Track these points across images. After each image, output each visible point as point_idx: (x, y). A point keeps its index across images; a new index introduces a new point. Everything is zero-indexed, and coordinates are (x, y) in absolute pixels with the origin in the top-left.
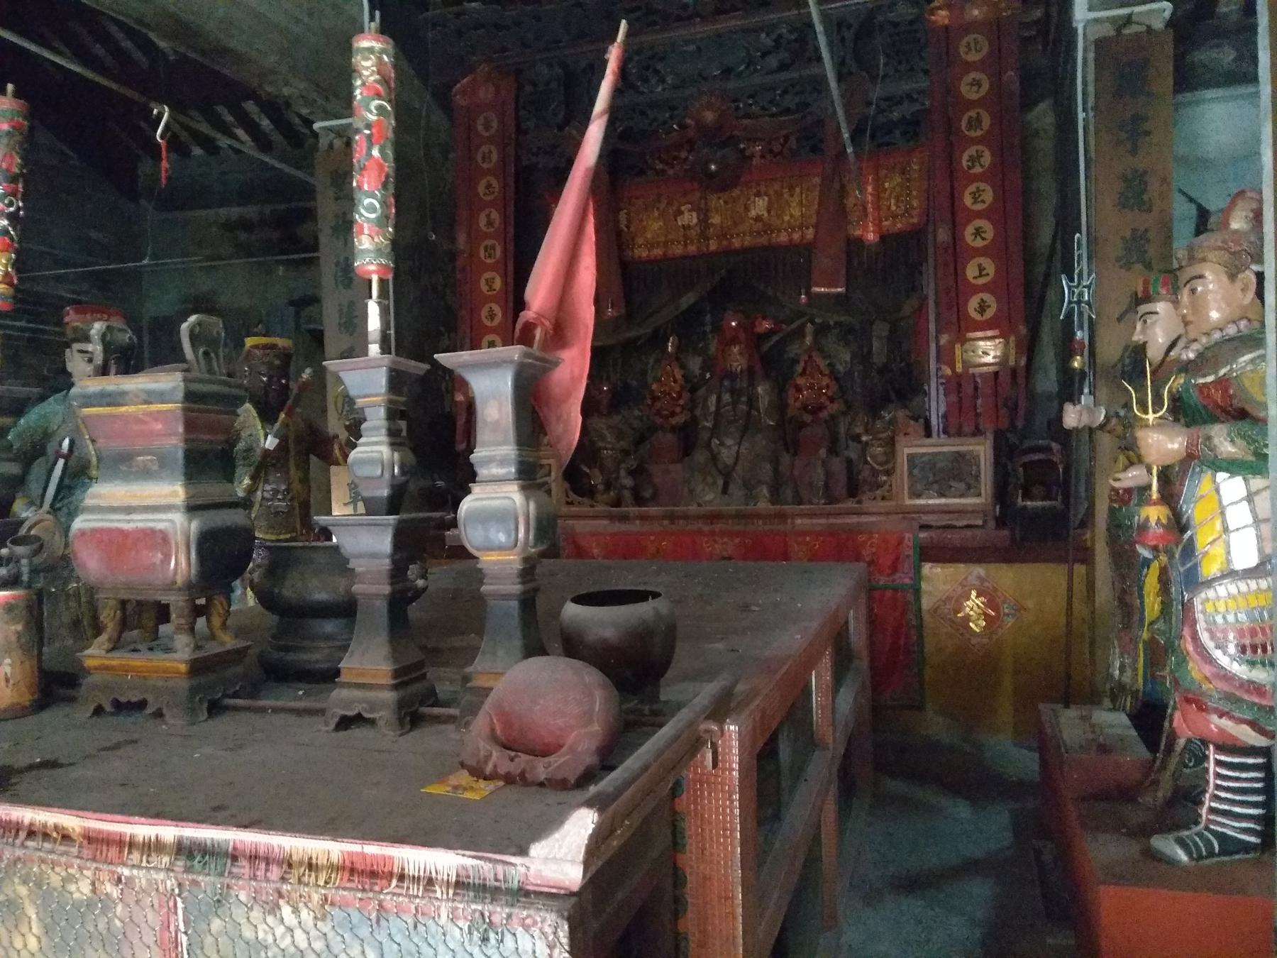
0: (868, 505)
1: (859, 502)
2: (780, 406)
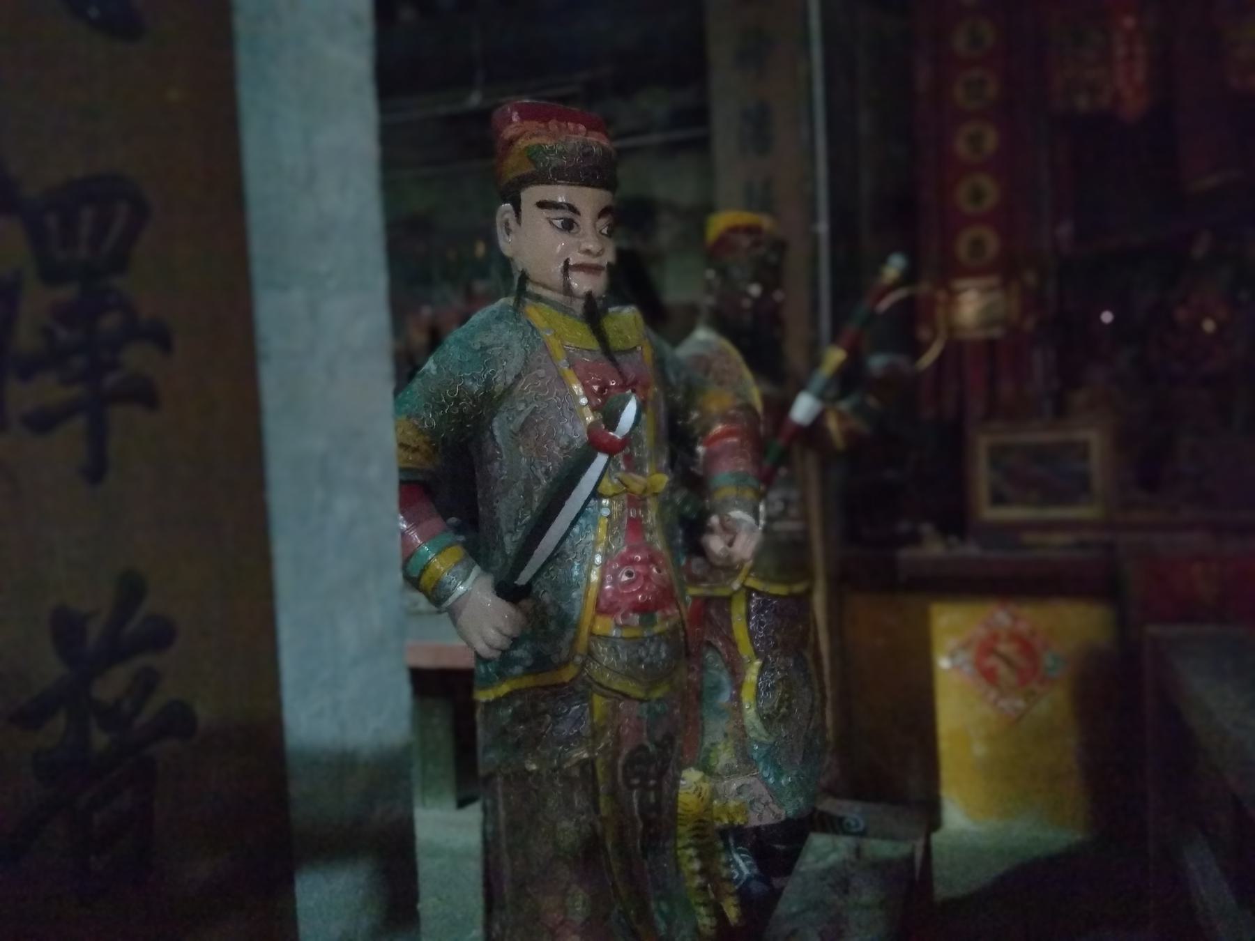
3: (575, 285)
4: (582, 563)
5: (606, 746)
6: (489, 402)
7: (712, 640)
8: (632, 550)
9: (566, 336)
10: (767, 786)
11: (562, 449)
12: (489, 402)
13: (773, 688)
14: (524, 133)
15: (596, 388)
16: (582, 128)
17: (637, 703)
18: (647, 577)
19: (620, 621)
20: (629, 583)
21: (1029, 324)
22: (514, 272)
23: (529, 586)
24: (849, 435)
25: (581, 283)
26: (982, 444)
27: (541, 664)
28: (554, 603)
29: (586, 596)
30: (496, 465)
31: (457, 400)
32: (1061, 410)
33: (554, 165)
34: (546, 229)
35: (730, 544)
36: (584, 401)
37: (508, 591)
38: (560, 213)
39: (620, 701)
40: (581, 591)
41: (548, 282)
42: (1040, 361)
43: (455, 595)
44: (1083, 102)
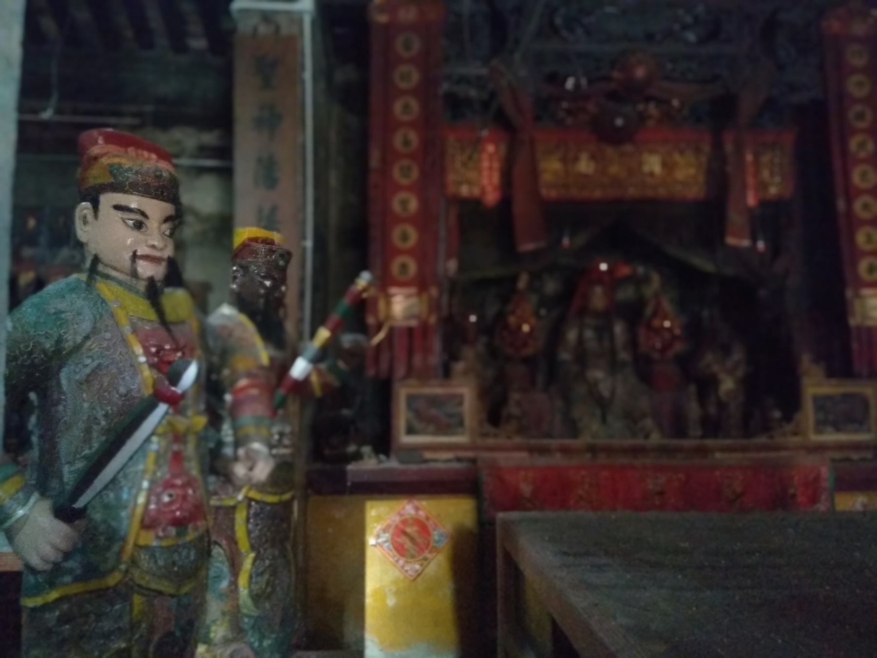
0: (779, 440)
1: (771, 437)
2: (633, 343)
3: (140, 270)
4: (130, 489)
5: (141, 636)
6: (59, 356)
7: (219, 541)
8: (175, 476)
9: (130, 308)
10: (253, 649)
11: (121, 396)
12: (59, 356)
13: (262, 574)
14: (104, 152)
15: (153, 350)
16: (154, 156)
17: (169, 598)
18: (185, 497)
19: (161, 534)
20: (170, 503)
21: (433, 320)
22: (87, 254)
23: (85, 508)
24: (325, 386)
25: (146, 269)
26: (402, 393)
27: (91, 571)
28: (105, 521)
29: (133, 515)
30: (61, 408)
31: (30, 353)
32: (447, 373)
33: (130, 180)
34: (120, 225)
35: (251, 469)
36: (143, 359)
37: (65, 512)
38: (132, 216)
39: (156, 597)
40: (129, 510)
41: (116, 265)
42: (437, 344)
43: (13, 519)
44: (465, 191)
